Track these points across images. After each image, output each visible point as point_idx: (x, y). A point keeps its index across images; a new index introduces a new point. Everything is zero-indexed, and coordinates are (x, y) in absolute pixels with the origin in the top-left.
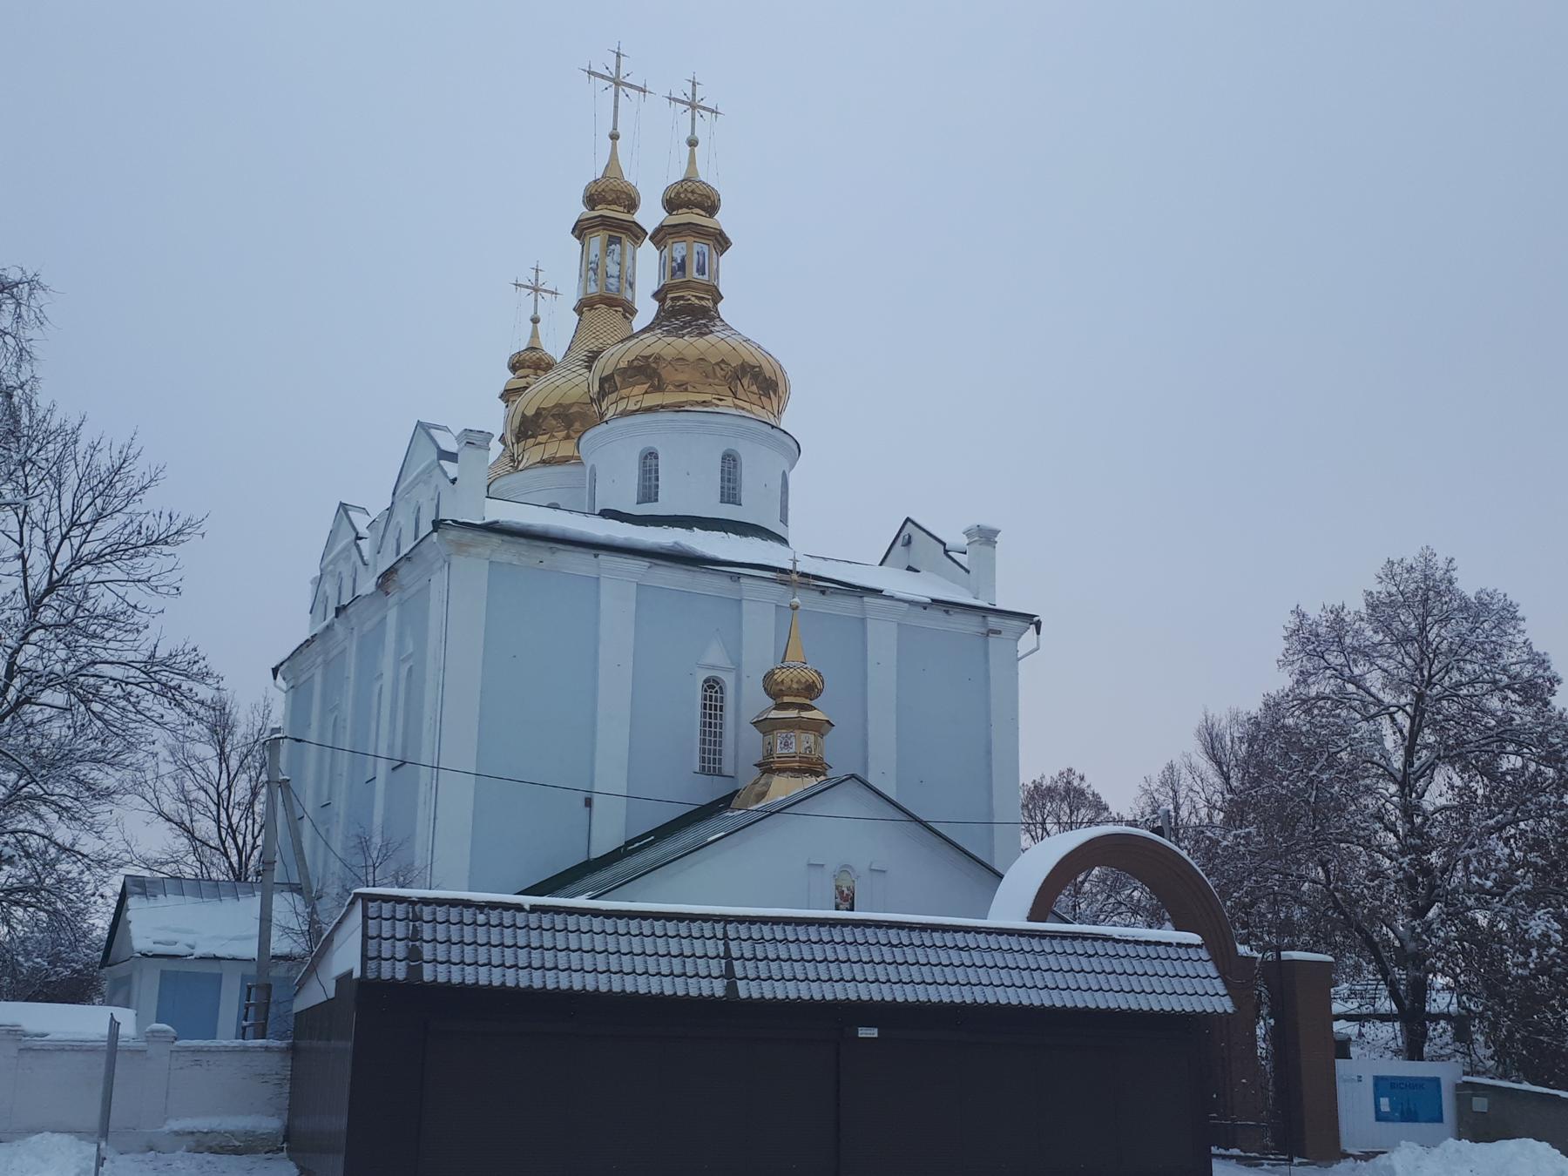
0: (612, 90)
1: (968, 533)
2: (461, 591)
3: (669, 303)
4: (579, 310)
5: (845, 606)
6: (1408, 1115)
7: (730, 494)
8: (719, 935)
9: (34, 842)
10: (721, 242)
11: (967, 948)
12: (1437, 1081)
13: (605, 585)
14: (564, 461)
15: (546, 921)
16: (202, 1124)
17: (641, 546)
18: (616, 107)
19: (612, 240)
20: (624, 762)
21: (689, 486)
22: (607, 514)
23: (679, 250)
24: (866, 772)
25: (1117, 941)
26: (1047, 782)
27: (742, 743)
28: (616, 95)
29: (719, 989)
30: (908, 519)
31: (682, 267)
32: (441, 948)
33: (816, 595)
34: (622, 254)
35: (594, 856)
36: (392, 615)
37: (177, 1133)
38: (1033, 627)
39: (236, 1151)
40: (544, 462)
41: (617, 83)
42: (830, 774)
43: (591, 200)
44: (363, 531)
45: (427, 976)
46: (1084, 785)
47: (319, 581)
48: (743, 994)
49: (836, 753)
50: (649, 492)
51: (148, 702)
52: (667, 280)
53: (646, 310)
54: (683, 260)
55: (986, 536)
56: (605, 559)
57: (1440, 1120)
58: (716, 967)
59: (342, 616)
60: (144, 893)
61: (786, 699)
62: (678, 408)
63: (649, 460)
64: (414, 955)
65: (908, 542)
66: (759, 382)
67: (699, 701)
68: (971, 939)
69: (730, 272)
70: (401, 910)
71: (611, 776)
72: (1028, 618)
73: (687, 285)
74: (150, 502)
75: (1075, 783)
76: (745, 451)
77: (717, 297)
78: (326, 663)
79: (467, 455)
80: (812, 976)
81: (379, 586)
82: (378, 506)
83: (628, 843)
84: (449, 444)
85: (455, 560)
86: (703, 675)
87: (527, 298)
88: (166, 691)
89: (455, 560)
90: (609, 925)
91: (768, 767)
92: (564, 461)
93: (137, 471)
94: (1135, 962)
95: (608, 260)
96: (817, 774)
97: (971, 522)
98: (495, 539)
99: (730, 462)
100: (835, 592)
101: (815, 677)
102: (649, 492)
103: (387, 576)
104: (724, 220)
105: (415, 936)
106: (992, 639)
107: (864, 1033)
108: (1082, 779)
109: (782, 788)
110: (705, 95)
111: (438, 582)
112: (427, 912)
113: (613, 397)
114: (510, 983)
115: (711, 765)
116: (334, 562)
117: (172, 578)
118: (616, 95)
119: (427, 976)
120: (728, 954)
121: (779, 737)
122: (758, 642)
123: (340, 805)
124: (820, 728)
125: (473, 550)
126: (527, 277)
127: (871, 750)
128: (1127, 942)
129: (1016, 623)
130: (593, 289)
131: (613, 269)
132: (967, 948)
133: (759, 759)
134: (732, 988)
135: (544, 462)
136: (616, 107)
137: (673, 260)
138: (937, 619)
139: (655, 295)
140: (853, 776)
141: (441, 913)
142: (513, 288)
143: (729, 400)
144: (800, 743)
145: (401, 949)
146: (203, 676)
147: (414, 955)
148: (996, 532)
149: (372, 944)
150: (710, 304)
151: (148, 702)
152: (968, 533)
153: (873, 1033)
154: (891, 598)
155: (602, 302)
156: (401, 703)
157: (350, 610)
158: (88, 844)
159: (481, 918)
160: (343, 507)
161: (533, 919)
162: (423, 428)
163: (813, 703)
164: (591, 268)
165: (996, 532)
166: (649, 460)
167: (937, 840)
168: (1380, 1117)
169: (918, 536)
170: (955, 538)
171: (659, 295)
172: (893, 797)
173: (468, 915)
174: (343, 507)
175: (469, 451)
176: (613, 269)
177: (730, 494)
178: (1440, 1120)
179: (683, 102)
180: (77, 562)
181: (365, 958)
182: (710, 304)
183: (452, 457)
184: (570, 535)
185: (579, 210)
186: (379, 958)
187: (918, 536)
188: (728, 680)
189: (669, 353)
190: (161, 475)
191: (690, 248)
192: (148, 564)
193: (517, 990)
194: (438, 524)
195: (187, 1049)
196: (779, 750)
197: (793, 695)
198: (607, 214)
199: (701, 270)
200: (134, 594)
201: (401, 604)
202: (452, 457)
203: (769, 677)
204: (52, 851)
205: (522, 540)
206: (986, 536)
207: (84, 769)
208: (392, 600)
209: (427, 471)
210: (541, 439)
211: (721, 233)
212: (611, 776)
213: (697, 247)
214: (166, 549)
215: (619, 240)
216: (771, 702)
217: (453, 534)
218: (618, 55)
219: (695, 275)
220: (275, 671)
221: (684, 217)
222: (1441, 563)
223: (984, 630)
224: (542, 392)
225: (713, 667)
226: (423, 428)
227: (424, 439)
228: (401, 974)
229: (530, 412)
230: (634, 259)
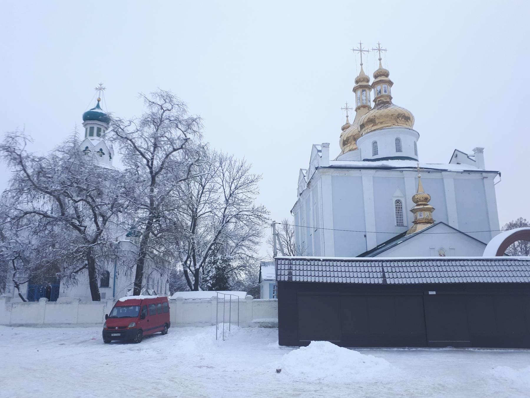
0: (360, 53)
1: (474, 150)
2: (325, 184)
3: (377, 102)
4: (356, 110)
5: (437, 175)
7: (399, 150)
8: (381, 265)
9: (243, 256)
10: (391, 83)
11: (464, 266)
14: (355, 149)
15: (327, 263)
16: (261, 320)
17: (372, 166)
19: (363, 91)
20: (375, 226)
21: (387, 148)
22: (364, 160)
23: (378, 88)
24: (448, 222)
25: (520, 261)
26: (514, 222)
27: (408, 217)
29: (381, 281)
31: (380, 92)
32: (298, 272)
33: (427, 173)
34: (366, 94)
35: (369, 250)
36: (311, 193)
37: (255, 323)
38: (498, 175)
39: (270, 327)
40: (350, 150)
41: (361, 51)
42: (435, 223)
43: (357, 82)
44: (305, 175)
45: (294, 279)
46: (526, 222)
47: (298, 189)
48: (388, 282)
49: (436, 216)
50: (375, 153)
51: (255, 220)
52: (376, 96)
53: (373, 105)
55: (480, 150)
56: (362, 171)
58: (379, 275)
60: (265, 265)
61: (419, 203)
62: (381, 129)
63: (375, 144)
64: (290, 274)
65: (457, 156)
66: (405, 118)
67: (394, 207)
68: (465, 263)
69: (394, 91)
70: (287, 262)
71: (370, 227)
72: (496, 172)
73: (382, 96)
74: (250, 172)
75: (523, 222)
76: (402, 137)
77: (391, 98)
78: (300, 208)
79: (324, 150)
80: (411, 276)
82: (307, 168)
83: (378, 246)
84: (319, 148)
88: (258, 217)
90: (346, 264)
91: (416, 222)
92: (355, 149)
93: (246, 165)
94: (526, 267)
95: (363, 96)
96: (431, 223)
98: (332, 170)
99: (398, 141)
100: (433, 172)
101: (428, 196)
102: (375, 153)
103: (309, 184)
104: (391, 78)
105: (290, 269)
107: (431, 293)
108: (525, 220)
109: (420, 227)
110: (383, 47)
111: (319, 183)
112: (294, 262)
114: (317, 281)
115: (400, 223)
116: (301, 183)
117: (257, 190)
119: (294, 279)
120: (383, 271)
121: (418, 214)
122: (410, 187)
123: (306, 242)
124: (431, 210)
127: (449, 215)
128: (523, 261)
129: (492, 174)
130: (359, 104)
131: (364, 98)
132: (464, 266)
133: (413, 220)
134: (385, 281)
135: (350, 150)
139: (374, 101)
140: (441, 222)
141: (298, 262)
142: (339, 108)
143: (396, 124)
144: (425, 215)
145: (287, 272)
146: (265, 212)
147: (290, 274)
148: (483, 149)
149: (279, 271)
150: (389, 100)
151: (255, 220)
152: (474, 150)
153: (434, 293)
155: (362, 107)
156: (315, 216)
158: (255, 256)
159: (309, 263)
160: (301, 170)
161: (324, 263)
162: (314, 146)
164: (358, 99)
165: (483, 149)
166: (375, 144)
167: (470, 239)
169: (459, 154)
170: (470, 152)
171: (375, 101)
172: (458, 229)
173: (305, 263)
174: (301, 170)
175: (324, 149)
176: (364, 98)
177: (399, 150)
180: (236, 188)
181: (277, 275)
182: (389, 100)
183: (320, 151)
185: (354, 85)
186: (281, 275)
187: (459, 154)
189: (377, 115)
191: (382, 88)
193: (331, 283)
194: (317, 168)
195: (256, 301)
196: (418, 217)
197: (421, 202)
198: (362, 84)
199: (385, 92)
200: (249, 195)
201: (313, 190)
202: (320, 151)
203: (414, 197)
204: (248, 258)
206: (480, 150)
207: (251, 238)
208: (311, 189)
209: (316, 156)
210: (349, 145)
212: (370, 227)
213: (383, 86)
214: (254, 183)
215: (365, 90)
216: (416, 204)
217: (321, 170)
220: (291, 211)
221: (379, 79)
224: (349, 132)
225: (398, 197)
226: (314, 146)
227: (315, 149)
228: (286, 279)
229: (345, 139)
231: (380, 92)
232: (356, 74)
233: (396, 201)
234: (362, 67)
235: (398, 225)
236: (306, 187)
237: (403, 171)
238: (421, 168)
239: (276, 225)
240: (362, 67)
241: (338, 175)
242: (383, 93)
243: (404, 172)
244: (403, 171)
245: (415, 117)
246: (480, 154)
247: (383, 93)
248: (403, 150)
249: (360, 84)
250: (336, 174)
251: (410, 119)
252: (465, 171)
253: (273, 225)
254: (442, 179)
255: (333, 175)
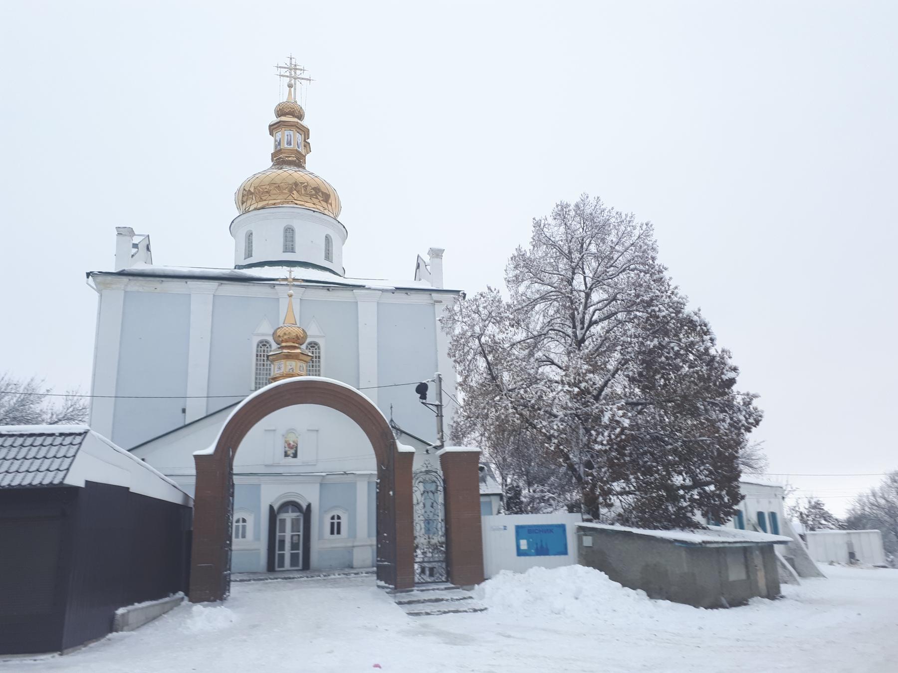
5: (345, 295)
6: (541, 550)
7: (289, 247)
12: (563, 527)
33: (325, 292)
55: (437, 254)
56: (192, 283)
57: (565, 552)
66: (321, 196)
76: (297, 225)
86: (256, 340)
98: (125, 279)
99: (289, 233)
106: (437, 305)
107: (391, 493)
125: (114, 286)
138: (401, 298)
154: (369, 289)
168: (520, 553)
177: (289, 247)
178: (565, 552)
184: (177, 274)
191: (283, 134)
199: (289, 143)
205: (140, 278)
213: (287, 133)
219: (286, 146)
221: (283, 118)
222: (592, 200)
225: (263, 335)
233: (261, 342)
234: (290, 91)
237: (274, 285)
238: (294, 280)
241: (141, 289)
244: (274, 285)
245: (340, 193)
246: (437, 260)
247: (285, 145)
248: (297, 249)
249: (283, 118)
250: (135, 288)
251: (332, 200)
255: (129, 289)
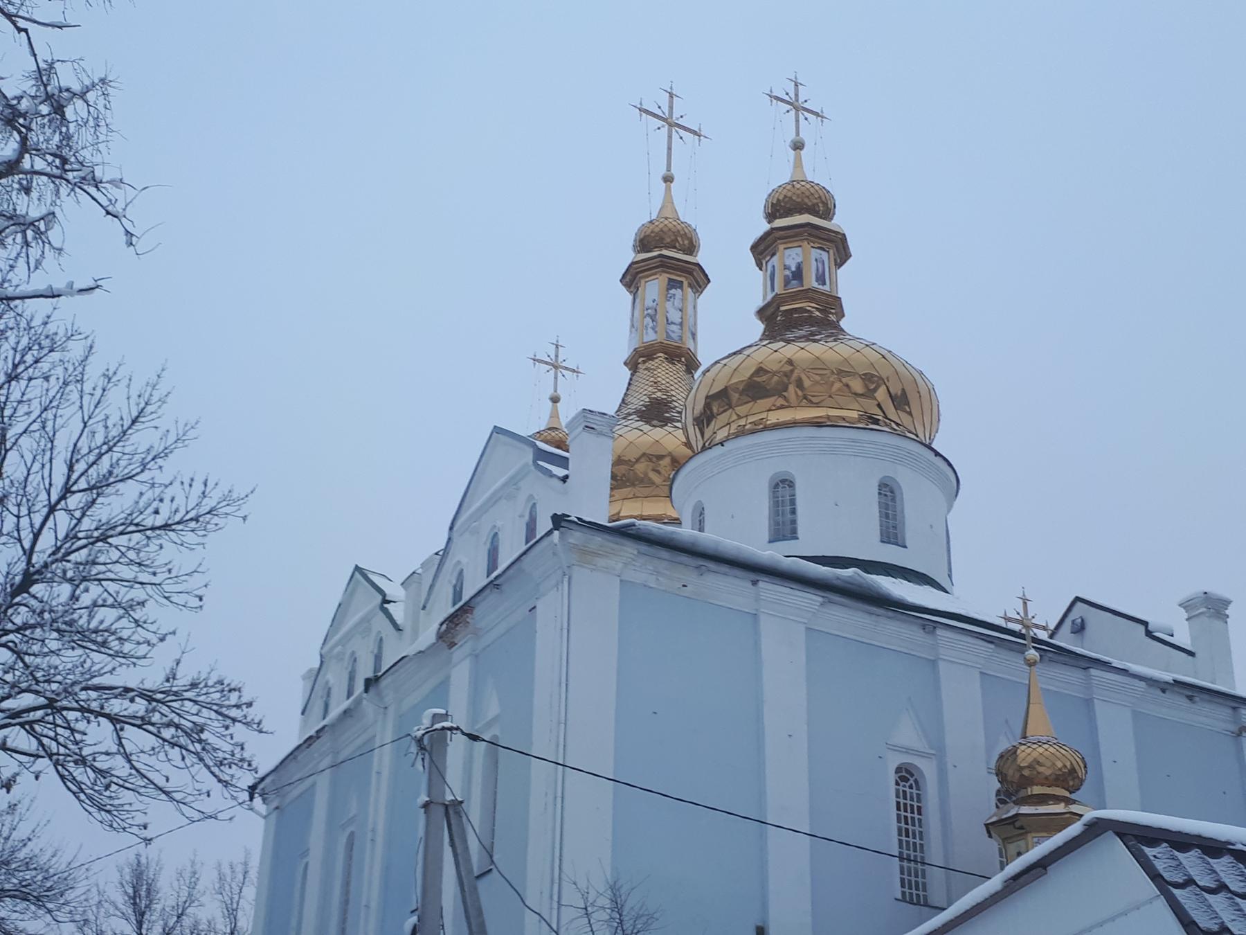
1: (1186, 605)
4: (633, 364)
13: (768, 626)
18: (669, 149)
19: (672, 284)
23: (791, 256)
28: (670, 137)
30: (1078, 599)
31: (798, 274)
34: (683, 300)
47: (316, 676)
52: (779, 289)
54: (799, 267)
55: (1211, 608)
56: (768, 588)
59: (372, 691)
63: (783, 487)
69: (848, 283)
81: (440, 636)
85: (580, 574)
86: (895, 760)
87: (546, 375)
89: (580, 574)
95: (669, 305)
97: (1193, 588)
98: (630, 549)
110: (568, 357)
111: (550, 608)
113: (723, 418)
117: (195, 583)
118: (670, 137)
125: (601, 562)
126: (783, 88)
130: (650, 337)
136: (669, 149)
137: (786, 267)
138: (1176, 709)
148: (1226, 603)
157: (384, 683)
163: (1073, 796)
166: (783, 487)
169: (1092, 615)
175: (587, 437)
176: (675, 316)
179: (546, 363)
185: (628, 256)
188: (927, 769)
190: (191, 434)
192: (166, 551)
205: (664, 554)
206: (1211, 608)
208: (457, 653)
211: (843, 238)
215: (679, 285)
217: (576, 537)
218: (671, 95)
219: (815, 284)
223: (1234, 728)
225: (907, 751)
230: (695, 307)
231: (798, 274)
232: (642, 211)
234: (668, 190)
235: (904, 900)
236: (428, 635)
239: (457, 744)
240: (668, 190)
242: (811, 281)
243: (939, 632)
246: (1218, 624)
252: (1177, 683)
253: (431, 746)
254: (1088, 703)
